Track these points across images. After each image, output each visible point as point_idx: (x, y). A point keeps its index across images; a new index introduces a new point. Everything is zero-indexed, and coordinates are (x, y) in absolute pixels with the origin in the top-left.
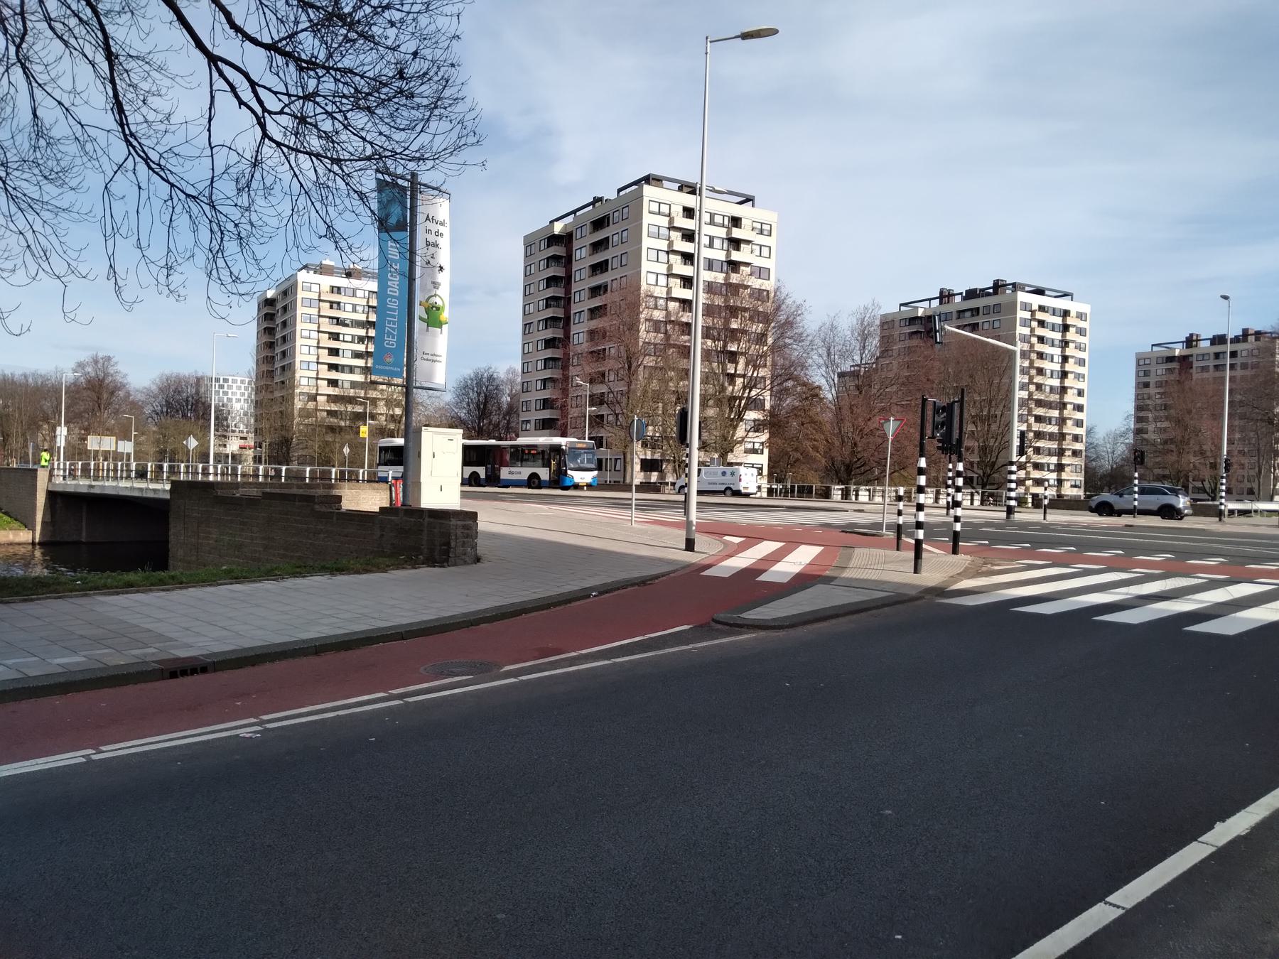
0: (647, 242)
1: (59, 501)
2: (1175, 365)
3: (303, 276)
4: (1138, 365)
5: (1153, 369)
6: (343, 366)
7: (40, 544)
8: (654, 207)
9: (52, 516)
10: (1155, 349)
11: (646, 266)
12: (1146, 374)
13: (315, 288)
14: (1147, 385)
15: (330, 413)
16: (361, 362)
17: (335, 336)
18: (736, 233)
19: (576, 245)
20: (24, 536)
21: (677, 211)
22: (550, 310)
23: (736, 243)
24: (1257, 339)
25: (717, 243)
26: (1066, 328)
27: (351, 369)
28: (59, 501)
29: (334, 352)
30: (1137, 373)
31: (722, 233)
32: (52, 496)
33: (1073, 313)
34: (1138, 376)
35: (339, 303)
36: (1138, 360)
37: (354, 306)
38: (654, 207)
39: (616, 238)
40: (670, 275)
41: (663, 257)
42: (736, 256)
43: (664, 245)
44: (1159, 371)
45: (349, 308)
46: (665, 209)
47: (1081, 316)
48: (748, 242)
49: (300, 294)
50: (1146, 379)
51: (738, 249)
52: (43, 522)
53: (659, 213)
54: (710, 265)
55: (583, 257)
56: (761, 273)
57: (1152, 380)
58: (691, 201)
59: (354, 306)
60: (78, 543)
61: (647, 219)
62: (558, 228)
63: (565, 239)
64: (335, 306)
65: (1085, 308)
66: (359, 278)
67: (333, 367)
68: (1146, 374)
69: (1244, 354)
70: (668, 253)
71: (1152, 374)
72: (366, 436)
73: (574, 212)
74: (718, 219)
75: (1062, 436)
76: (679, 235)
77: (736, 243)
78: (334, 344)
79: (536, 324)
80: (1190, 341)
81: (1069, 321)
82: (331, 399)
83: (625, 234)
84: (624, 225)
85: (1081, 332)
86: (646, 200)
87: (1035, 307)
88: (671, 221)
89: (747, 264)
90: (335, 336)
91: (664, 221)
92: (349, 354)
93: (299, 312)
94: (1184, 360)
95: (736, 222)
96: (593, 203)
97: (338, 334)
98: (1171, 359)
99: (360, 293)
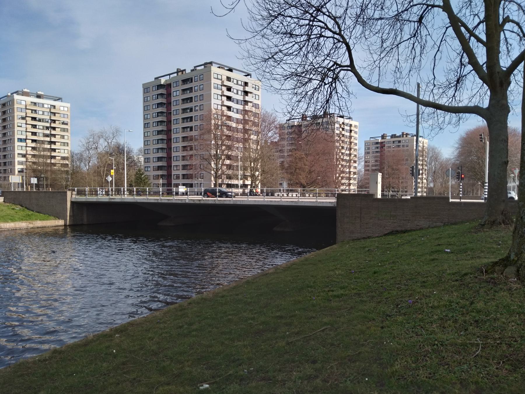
0: (213, 91)
1: (75, 206)
2: (379, 145)
3: (16, 97)
4: (365, 145)
5: (371, 147)
6: (39, 141)
7: (69, 225)
8: (216, 76)
9: (73, 213)
10: (371, 139)
11: (213, 101)
12: (369, 149)
13: (23, 103)
14: (368, 153)
15: (34, 163)
16: (48, 139)
17: (34, 126)
18: (247, 89)
19: (173, 89)
20: (61, 222)
21: (224, 78)
22: (159, 117)
23: (246, 93)
24: (406, 136)
25: (240, 92)
26: (351, 131)
27: (43, 142)
28: (75, 206)
29: (34, 134)
30: (365, 148)
31: (241, 88)
32: (73, 203)
33: (353, 126)
34: (365, 149)
35: (35, 111)
36: (365, 144)
37: (43, 112)
38: (216, 76)
39: (196, 88)
40: (222, 105)
41: (220, 97)
42: (247, 98)
43: (220, 92)
44: (373, 148)
45: (41, 113)
46: (220, 77)
47: (355, 126)
48: (251, 93)
49: (16, 106)
50: (368, 151)
51: (247, 95)
52: (70, 216)
53: (217, 79)
54: (237, 102)
55: (177, 95)
56: (256, 106)
57: (371, 151)
58: (229, 74)
59: (43, 112)
60: (82, 225)
61: (213, 81)
62: (163, 81)
63: (168, 86)
64: (33, 112)
65: (357, 124)
66: (43, 98)
67: (34, 119)
68: (369, 149)
69: (403, 141)
70: (221, 96)
71: (371, 149)
72: (113, 174)
73: (169, 75)
74: (240, 83)
75: (350, 172)
76: (30, 156)
77: (246, 93)
78: (34, 130)
79: (151, 124)
80: (383, 137)
81: (352, 129)
82: (34, 156)
83: (201, 87)
84: (201, 83)
85: (356, 133)
86: (212, 72)
87: (341, 123)
88: (223, 82)
89: (251, 102)
90: (34, 126)
91: (219, 82)
92: (41, 135)
93: (16, 114)
94: (382, 145)
95: (246, 84)
96: (177, 72)
97: (36, 125)
98: (377, 143)
99: (46, 106)
